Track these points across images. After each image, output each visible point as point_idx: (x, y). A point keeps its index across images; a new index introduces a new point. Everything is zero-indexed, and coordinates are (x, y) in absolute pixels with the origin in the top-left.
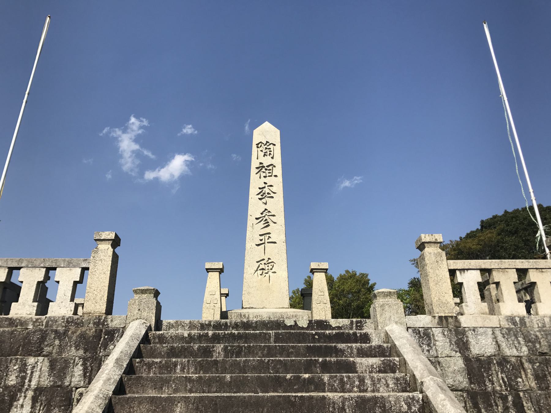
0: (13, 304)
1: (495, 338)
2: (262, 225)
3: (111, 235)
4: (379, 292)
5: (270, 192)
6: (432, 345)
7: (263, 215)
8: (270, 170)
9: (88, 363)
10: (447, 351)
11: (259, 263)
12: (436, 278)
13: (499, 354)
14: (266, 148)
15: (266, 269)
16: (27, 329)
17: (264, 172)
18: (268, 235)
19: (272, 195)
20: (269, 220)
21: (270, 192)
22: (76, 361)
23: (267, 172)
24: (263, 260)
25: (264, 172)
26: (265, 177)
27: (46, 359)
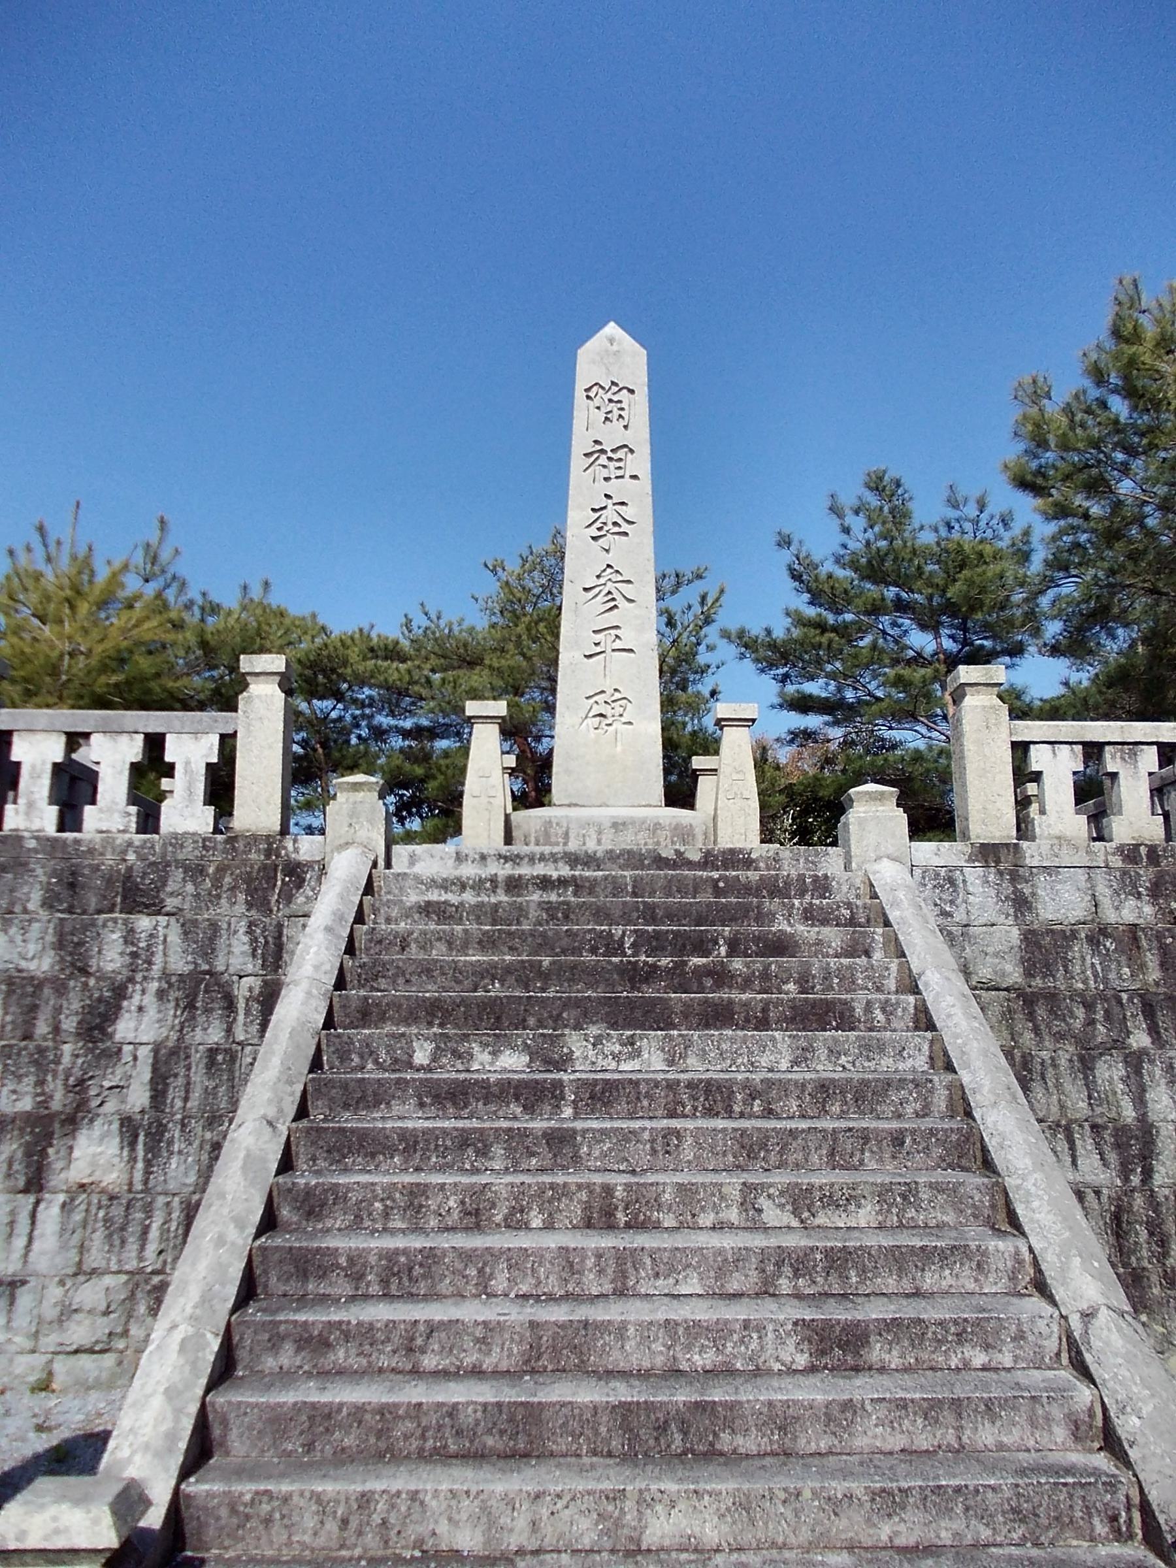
0: (88, 809)
1: (1093, 887)
2: (599, 604)
3: (277, 662)
4: (858, 793)
5: (620, 521)
6: (959, 901)
7: (602, 581)
8: (620, 460)
9: (258, 931)
10: (990, 915)
11: (592, 701)
12: (982, 763)
13: (1093, 921)
14: (610, 401)
15: (609, 715)
16: (125, 860)
17: (604, 466)
18: (613, 632)
19: (625, 527)
20: (616, 595)
21: (620, 521)
22: (233, 926)
23: (612, 465)
24: (603, 692)
25: (604, 466)
26: (607, 479)
27: (173, 919)
